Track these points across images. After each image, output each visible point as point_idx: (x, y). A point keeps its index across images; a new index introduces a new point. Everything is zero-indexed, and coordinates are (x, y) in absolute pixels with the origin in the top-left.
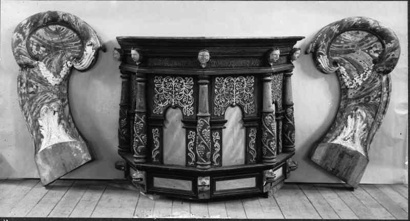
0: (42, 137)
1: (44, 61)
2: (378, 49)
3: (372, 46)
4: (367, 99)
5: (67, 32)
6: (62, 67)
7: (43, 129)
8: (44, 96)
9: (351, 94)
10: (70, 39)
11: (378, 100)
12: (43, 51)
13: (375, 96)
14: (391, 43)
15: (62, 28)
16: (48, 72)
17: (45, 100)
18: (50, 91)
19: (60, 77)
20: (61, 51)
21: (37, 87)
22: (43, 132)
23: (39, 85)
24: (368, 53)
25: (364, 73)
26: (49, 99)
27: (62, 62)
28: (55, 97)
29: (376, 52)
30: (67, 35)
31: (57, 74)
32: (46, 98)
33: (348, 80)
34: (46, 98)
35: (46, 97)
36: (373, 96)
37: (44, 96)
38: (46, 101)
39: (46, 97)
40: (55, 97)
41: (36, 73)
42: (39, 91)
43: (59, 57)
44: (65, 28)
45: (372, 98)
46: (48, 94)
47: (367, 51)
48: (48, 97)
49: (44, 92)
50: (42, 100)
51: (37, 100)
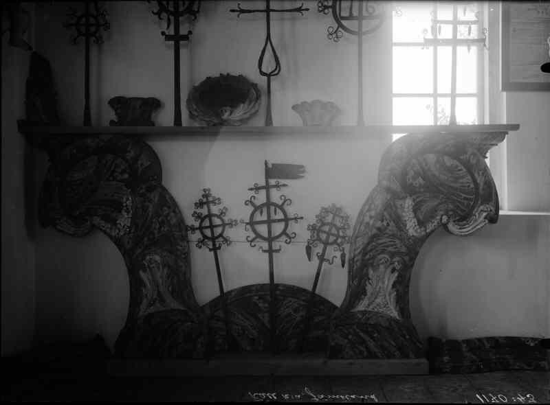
0: (364, 293)
1: (414, 197)
2: (123, 167)
3: (113, 168)
4: (151, 237)
5: (463, 177)
6: (433, 217)
7: (370, 284)
8: (390, 241)
9: (128, 242)
10: (463, 188)
11: (165, 229)
12: (420, 185)
13: (158, 226)
14: (130, 152)
15: (459, 168)
16: (412, 215)
17: (387, 246)
18: (401, 240)
19: (426, 230)
20: (442, 196)
21: (388, 225)
22: (369, 288)
23: (392, 224)
24: (114, 179)
25: (125, 208)
26: (396, 248)
27: (436, 211)
28: (404, 250)
29: (123, 172)
30: (461, 181)
31: (421, 223)
32: (392, 246)
33: (111, 229)
34: (392, 246)
35: (392, 243)
36: (155, 228)
37: (390, 241)
38: (390, 249)
39: (392, 243)
40: (404, 250)
41: (396, 208)
42: (387, 231)
43: (436, 203)
44: (464, 170)
45: (156, 231)
46: (397, 242)
47: (111, 178)
48: (395, 245)
49: (394, 236)
50: (385, 244)
51: (380, 241)
